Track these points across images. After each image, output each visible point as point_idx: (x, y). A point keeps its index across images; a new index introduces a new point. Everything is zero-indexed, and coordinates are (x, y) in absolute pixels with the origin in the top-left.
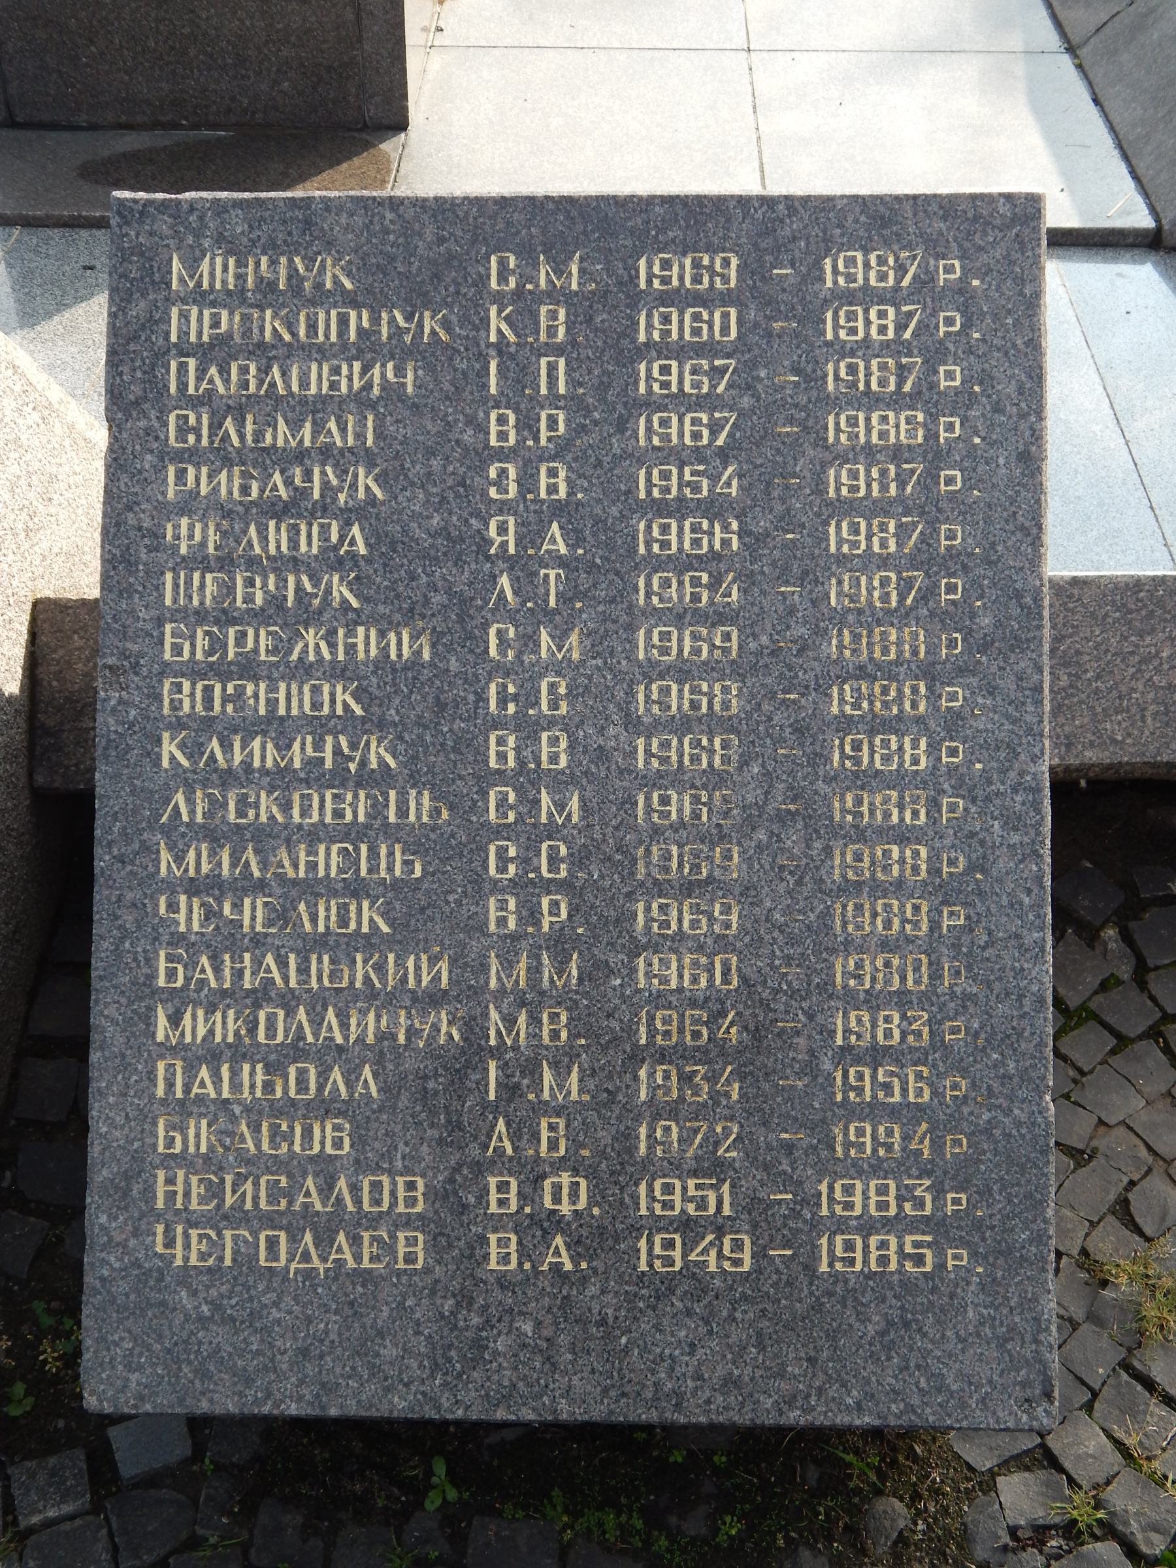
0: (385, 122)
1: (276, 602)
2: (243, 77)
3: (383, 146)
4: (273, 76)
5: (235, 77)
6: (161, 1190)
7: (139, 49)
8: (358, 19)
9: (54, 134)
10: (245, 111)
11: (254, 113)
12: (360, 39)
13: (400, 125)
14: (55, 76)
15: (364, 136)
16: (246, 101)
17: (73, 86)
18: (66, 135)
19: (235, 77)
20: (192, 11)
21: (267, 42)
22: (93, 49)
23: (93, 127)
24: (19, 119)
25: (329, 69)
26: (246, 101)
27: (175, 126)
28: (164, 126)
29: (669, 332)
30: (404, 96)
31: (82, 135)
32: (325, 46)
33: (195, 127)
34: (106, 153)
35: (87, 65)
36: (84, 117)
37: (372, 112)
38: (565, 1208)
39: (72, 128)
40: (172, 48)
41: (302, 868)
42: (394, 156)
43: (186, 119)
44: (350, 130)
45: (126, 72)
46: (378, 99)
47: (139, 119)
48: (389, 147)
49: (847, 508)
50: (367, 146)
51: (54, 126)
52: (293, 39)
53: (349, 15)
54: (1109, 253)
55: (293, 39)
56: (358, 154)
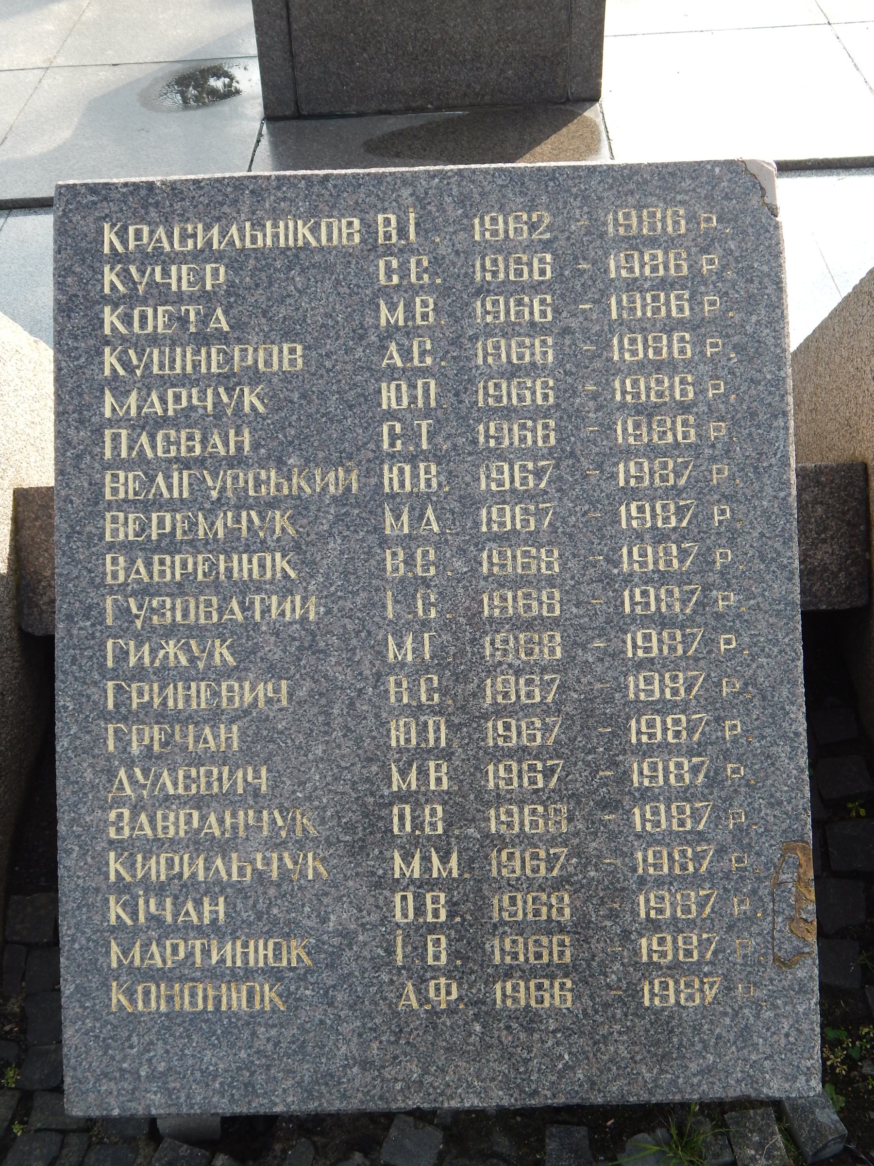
0: (583, 95)
1: (232, 534)
2: (478, 69)
3: (586, 114)
4: (501, 66)
5: (471, 69)
6: (221, 908)
7: (401, 52)
8: (570, 19)
9: (332, 122)
10: (477, 94)
11: (483, 96)
12: (569, 35)
13: (594, 97)
14: (334, 78)
15: (568, 107)
16: (478, 88)
17: (347, 85)
18: (341, 122)
19: (471, 69)
20: (443, 22)
21: (498, 41)
22: (365, 55)
23: (360, 115)
24: (305, 113)
25: (544, 58)
26: (478, 88)
27: (422, 109)
28: (414, 110)
29: (193, 354)
30: (599, 75)
31: (353, 121)
32: (543, 41)
33: (438, 109)
34: (379, 133)
35: (360, 68)
36: (354, 107)
37: (574, 89)
38: (443, 981)
39: (344, 116)
40: (425, 50)
41: (181, 786)
42: (599, 120)
43: (432, 103)
44: (556, 103)
45: (389, 72)
46: (579, 79)
47: (396, 106)
48: (591, 113)
49: (630, 494)
50: (574, 115)
51: (330, 116)
52: (519, 37)
53: (564, 17)
54: (828, 171)
55: (519, 37)
56: (571, 121)
